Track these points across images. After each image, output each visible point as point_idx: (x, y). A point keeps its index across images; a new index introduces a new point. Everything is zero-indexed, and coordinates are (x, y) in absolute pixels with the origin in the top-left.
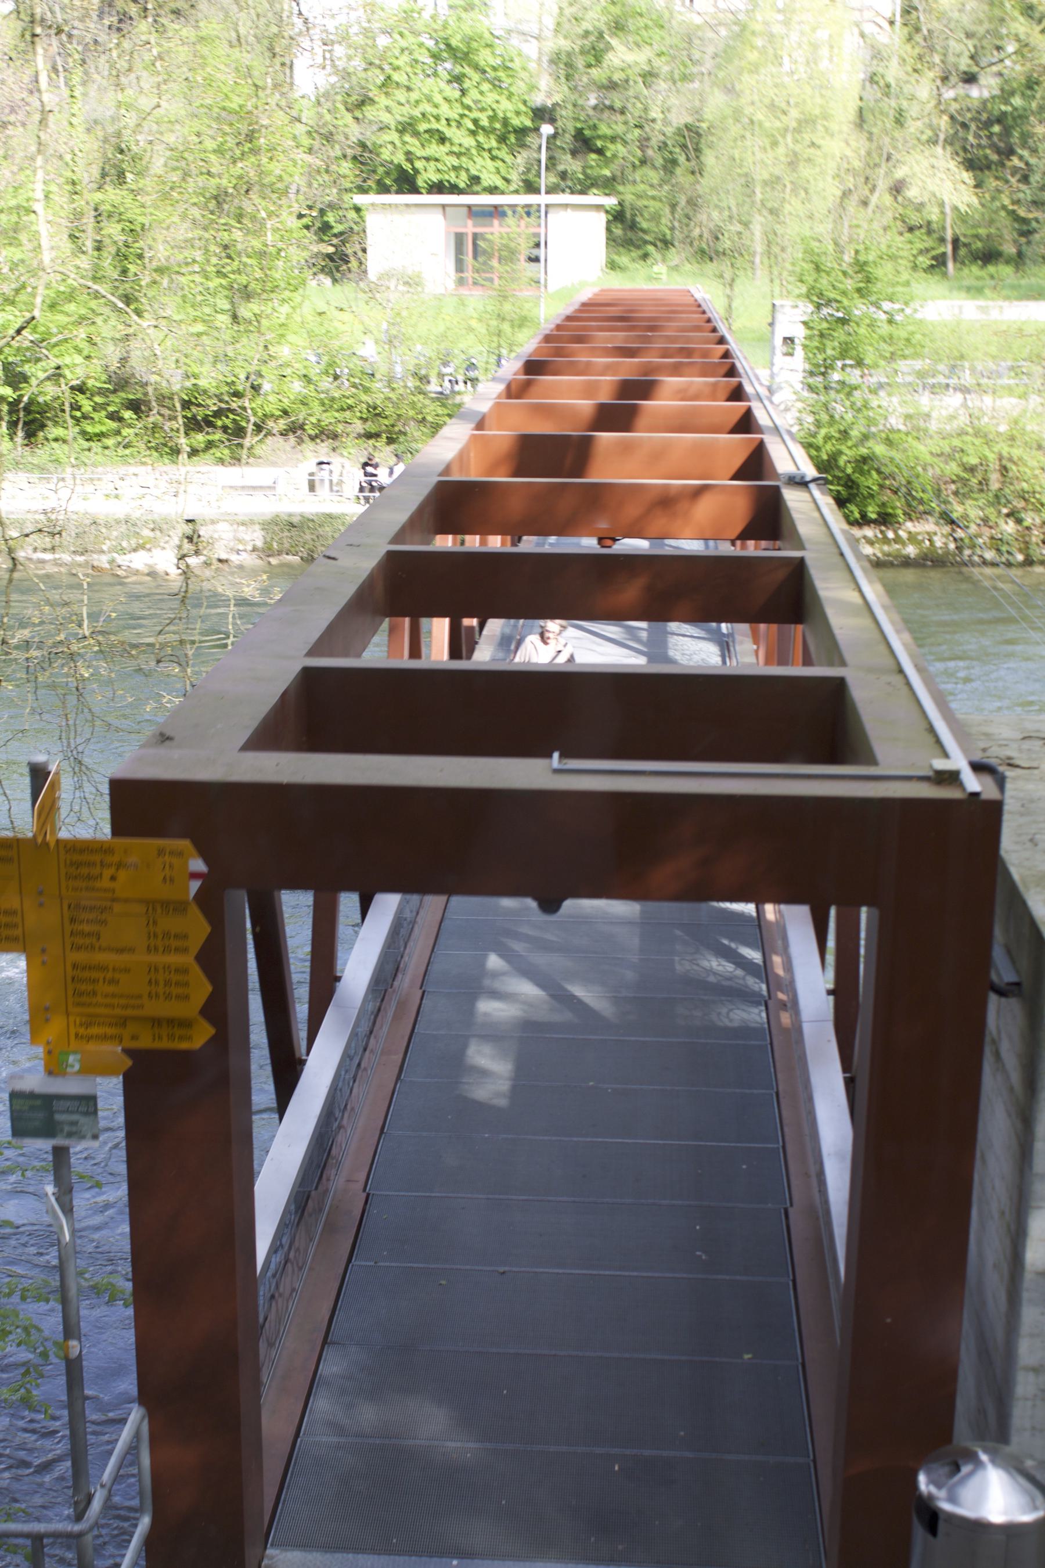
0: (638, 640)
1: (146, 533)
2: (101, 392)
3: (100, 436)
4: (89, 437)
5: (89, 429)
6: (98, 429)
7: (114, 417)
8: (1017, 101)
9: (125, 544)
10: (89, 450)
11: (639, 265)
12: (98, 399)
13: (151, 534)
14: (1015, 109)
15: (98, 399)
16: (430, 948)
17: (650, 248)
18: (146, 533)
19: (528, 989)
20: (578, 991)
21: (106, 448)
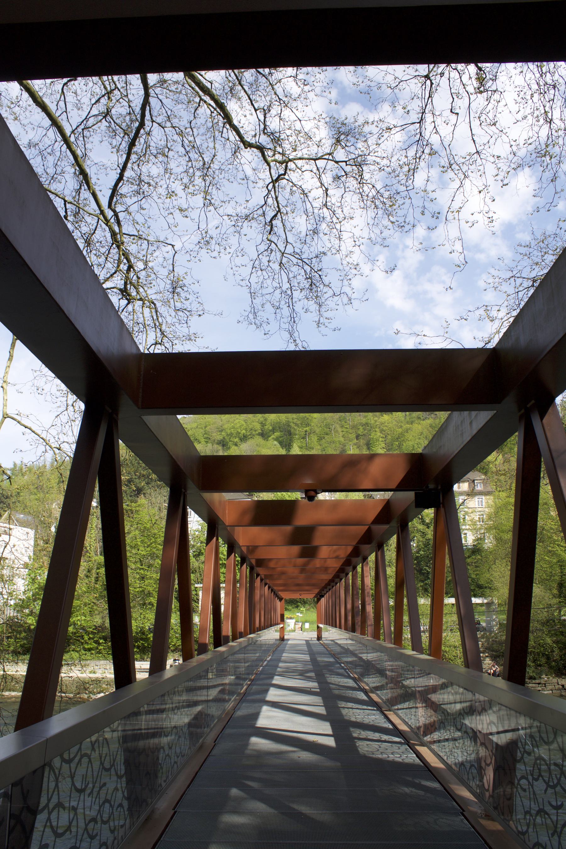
0: (313, 679)
1: (104, 686)
2: (93, 633)
3: (90, 650)
4: (85, 650)
5: (86, 647)
6: (89, 646)
7: (97, 642)
8: (422, 553)
9: (95, 690)
10: (86, 655)
11: (296, 610)
12: (91, 636)
13: (106, 687)
14: (421, 555)
15: (91, 636)
16: (186, 786)
17: (299, 604)
18: (104, 686)
19: (260, 806)
20: (304, 809)
21: (92, 654)
